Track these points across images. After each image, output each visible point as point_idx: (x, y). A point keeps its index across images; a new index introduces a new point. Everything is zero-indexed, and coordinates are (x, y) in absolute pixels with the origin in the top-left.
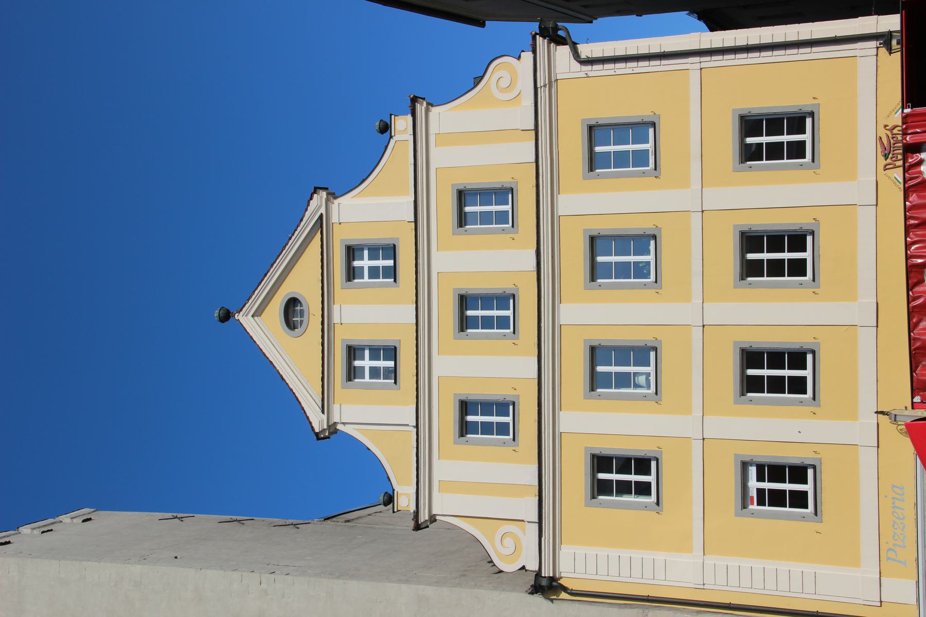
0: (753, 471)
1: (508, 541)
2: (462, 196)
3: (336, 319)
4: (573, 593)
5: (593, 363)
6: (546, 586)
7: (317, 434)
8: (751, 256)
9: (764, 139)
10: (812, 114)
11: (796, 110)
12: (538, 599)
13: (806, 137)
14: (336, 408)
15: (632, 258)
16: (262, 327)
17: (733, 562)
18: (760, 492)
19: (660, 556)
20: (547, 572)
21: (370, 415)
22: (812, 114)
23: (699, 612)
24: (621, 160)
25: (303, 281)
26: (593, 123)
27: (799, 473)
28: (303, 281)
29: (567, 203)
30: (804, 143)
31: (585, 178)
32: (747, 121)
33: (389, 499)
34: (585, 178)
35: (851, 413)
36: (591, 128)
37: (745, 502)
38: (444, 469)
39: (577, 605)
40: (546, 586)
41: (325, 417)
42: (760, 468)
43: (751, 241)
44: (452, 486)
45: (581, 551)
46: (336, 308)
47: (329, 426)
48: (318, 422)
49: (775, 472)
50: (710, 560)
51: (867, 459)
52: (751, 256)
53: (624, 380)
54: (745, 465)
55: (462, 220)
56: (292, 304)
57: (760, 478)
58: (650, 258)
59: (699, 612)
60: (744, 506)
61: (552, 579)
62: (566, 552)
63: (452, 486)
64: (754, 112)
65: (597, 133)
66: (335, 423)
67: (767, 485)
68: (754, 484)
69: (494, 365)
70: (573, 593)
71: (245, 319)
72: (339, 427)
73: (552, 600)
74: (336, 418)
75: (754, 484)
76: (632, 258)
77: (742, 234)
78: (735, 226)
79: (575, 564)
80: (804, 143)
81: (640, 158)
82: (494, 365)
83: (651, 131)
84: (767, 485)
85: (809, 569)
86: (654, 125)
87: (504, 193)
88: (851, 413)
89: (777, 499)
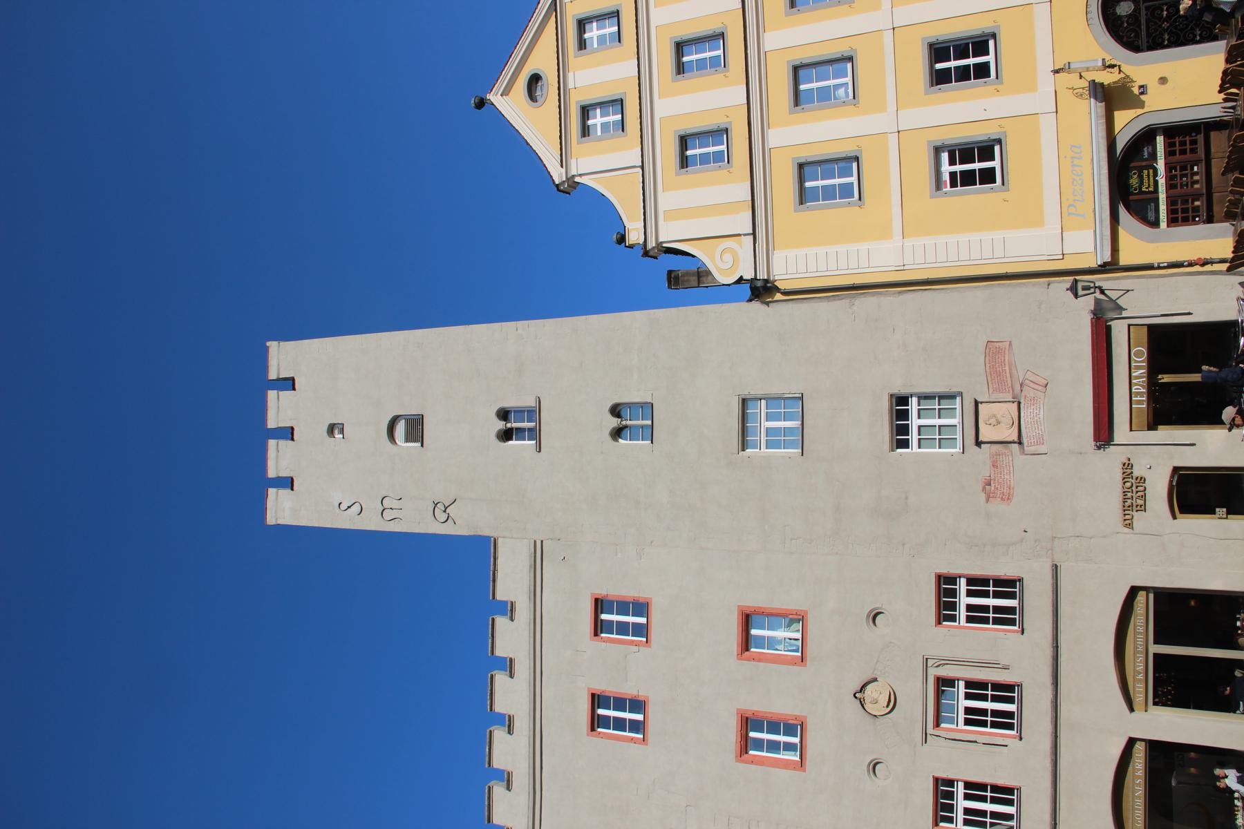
0: (945, 157)
1: (728, 257)
2: (680, 47)
3: (571, 85)
4: (786, 293)
5: (801, 180)
6: (761, 290)
7: (557, 186)
8: (939, 66)
9: (952, 64)
10: (999, 141)
11: (980, 32)
12: (756, 305)
13: (990, 58)
14: (573, 163)
15: (837, 181)
16: (510, 104)
17: (929, 241)
18: (953, 175)
19: (864, 247)
20: (762, 275)
21: (601, 164)
22: (999, 141)
23: (900, 293)
24: (829, 193)
25: (542, 60)
26: (798, 63)
27: (986, 151)
28: (542, 60)
29: (776, 137)
30: (993, 169)
31: (787, 15)
32: (936, 50)
33: (622, 239)
34: (787, 15)
35: (1032, 86)
36: (801, 166)
37: (938, 185)
38: (667, 200)
39: (790, 305)
40: (761, 290)
41: (563, 170)
42: (971, 581)
43: (938, 51)
44: (675, 214)
45: (792, 253)
46: (570, 76)
47: (568, 179)
48: (558, 175)
49: (963, 153)
50: (909, 242)
51: (1047, 125)
52: (939, 66)
53: (825, 95)
54: (938, 150)
55: (684, 162)
56: (535, 79)
57: (952, 162)
58: (853, 179)
59: (900, 293)
60: (938, 188)
61: (766, 281)
62: (778, 258)
63: (675, 214)
64: (941, 39)
65: (802, 73)
66: (573, 176)
67: (959, 168)
68: (946, 168)
69: (711, 99)
70: (786, 293)
71: (494, 98)
72: (577, 179)
73: (767, 304)
74: (574, 172)
75: (946, 168)
76: (837, 181)
77: (931, 45)
78: (929, 142)
79: (787, 267)
80: (993, 169)
81: (846, 191)
82: (711, 99)
83: (855, 165)
84: (959, 168)
85: (998, 235)
86: (857, 159)
87: (720, 133)
88: (1032, 86)
89: (967, 179)
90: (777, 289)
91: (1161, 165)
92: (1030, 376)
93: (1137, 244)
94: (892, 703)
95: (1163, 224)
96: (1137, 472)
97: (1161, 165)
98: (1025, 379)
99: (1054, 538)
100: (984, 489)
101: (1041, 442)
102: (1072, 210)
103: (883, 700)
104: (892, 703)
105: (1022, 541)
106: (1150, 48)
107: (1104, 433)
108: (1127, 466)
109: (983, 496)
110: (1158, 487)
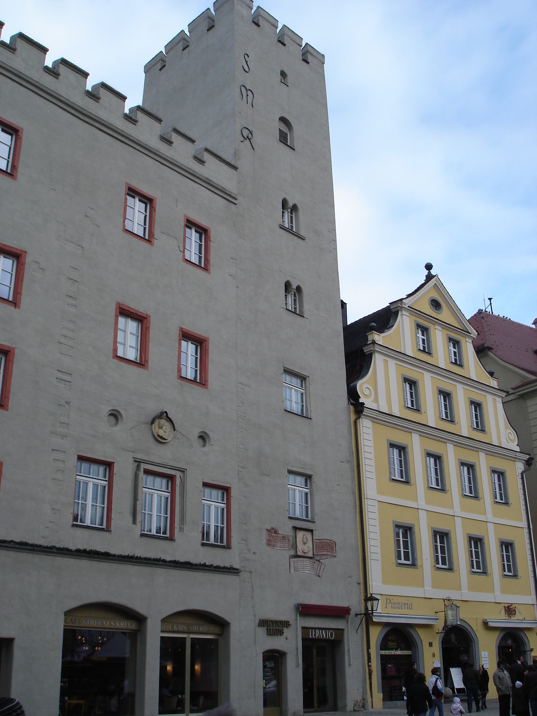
30: (77, 522)
70: (355, 423)
80: (77, 522)
90: (359, 418)
91: (399, 652)
92: (323, 566)
93: (376, 634)
94: (160, 440)
95: (383, 652)
96: (285, 630)
97: (399, 652)
98: (322, 563)
99: (251, 572)
100: (273, 529)
101: (296, 570)
102: (388, 601)
103: (161, 432)
104: (160, 440)
105: (249, 551)
106: (382, 677)
107: (305, 610)
108: (286, 624)
109: (269, 528)
110: (276, 643)
